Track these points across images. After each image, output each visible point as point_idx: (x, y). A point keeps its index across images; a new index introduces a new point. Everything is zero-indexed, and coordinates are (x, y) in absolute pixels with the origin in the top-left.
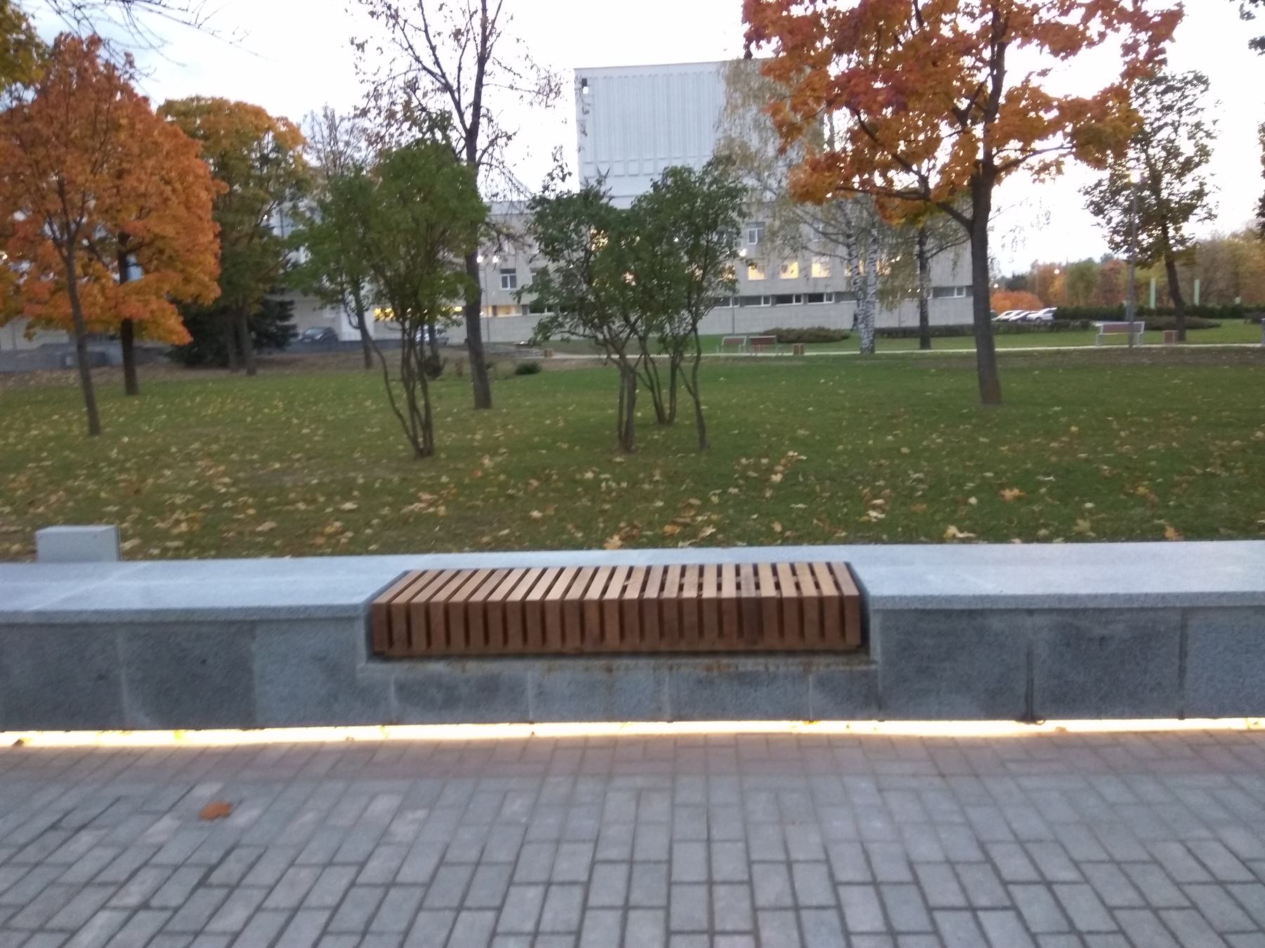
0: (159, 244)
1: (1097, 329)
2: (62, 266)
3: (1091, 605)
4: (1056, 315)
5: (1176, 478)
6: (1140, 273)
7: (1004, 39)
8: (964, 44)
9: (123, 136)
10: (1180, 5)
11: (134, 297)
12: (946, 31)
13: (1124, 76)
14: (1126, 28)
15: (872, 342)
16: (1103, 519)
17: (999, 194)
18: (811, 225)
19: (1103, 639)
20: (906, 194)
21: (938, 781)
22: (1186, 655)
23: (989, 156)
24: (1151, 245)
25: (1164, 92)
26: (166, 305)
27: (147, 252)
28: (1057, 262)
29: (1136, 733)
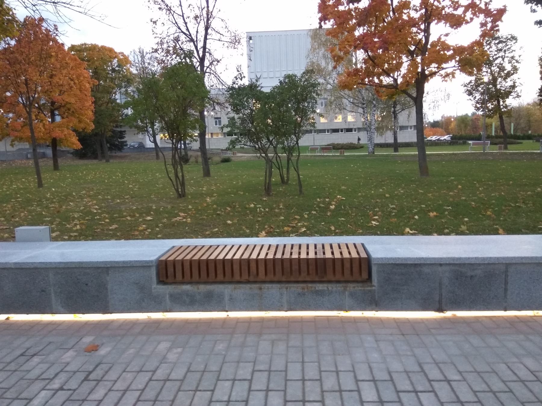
0: (68, 106)
1: (470, 144)
2: (27, 115)
3: (467, 262)
4: (452, 138)
5: (503, 208)
6: (488, 120)
7: (430, 20)
9: (53, 60)
10: (505, 6)
11: (57, 129)
12: (405, 17)
14: (482, 16)
15: (373, 149)
17: (428, 86)
19: (472, 276)
20: (388, 86)
21: (401, 337)
22: (507, 283)
24: (493, 108)
25: (498, 43)
26: (71, 132)
27: (63, 109)
28: (452, 115)
29: (486, 317)
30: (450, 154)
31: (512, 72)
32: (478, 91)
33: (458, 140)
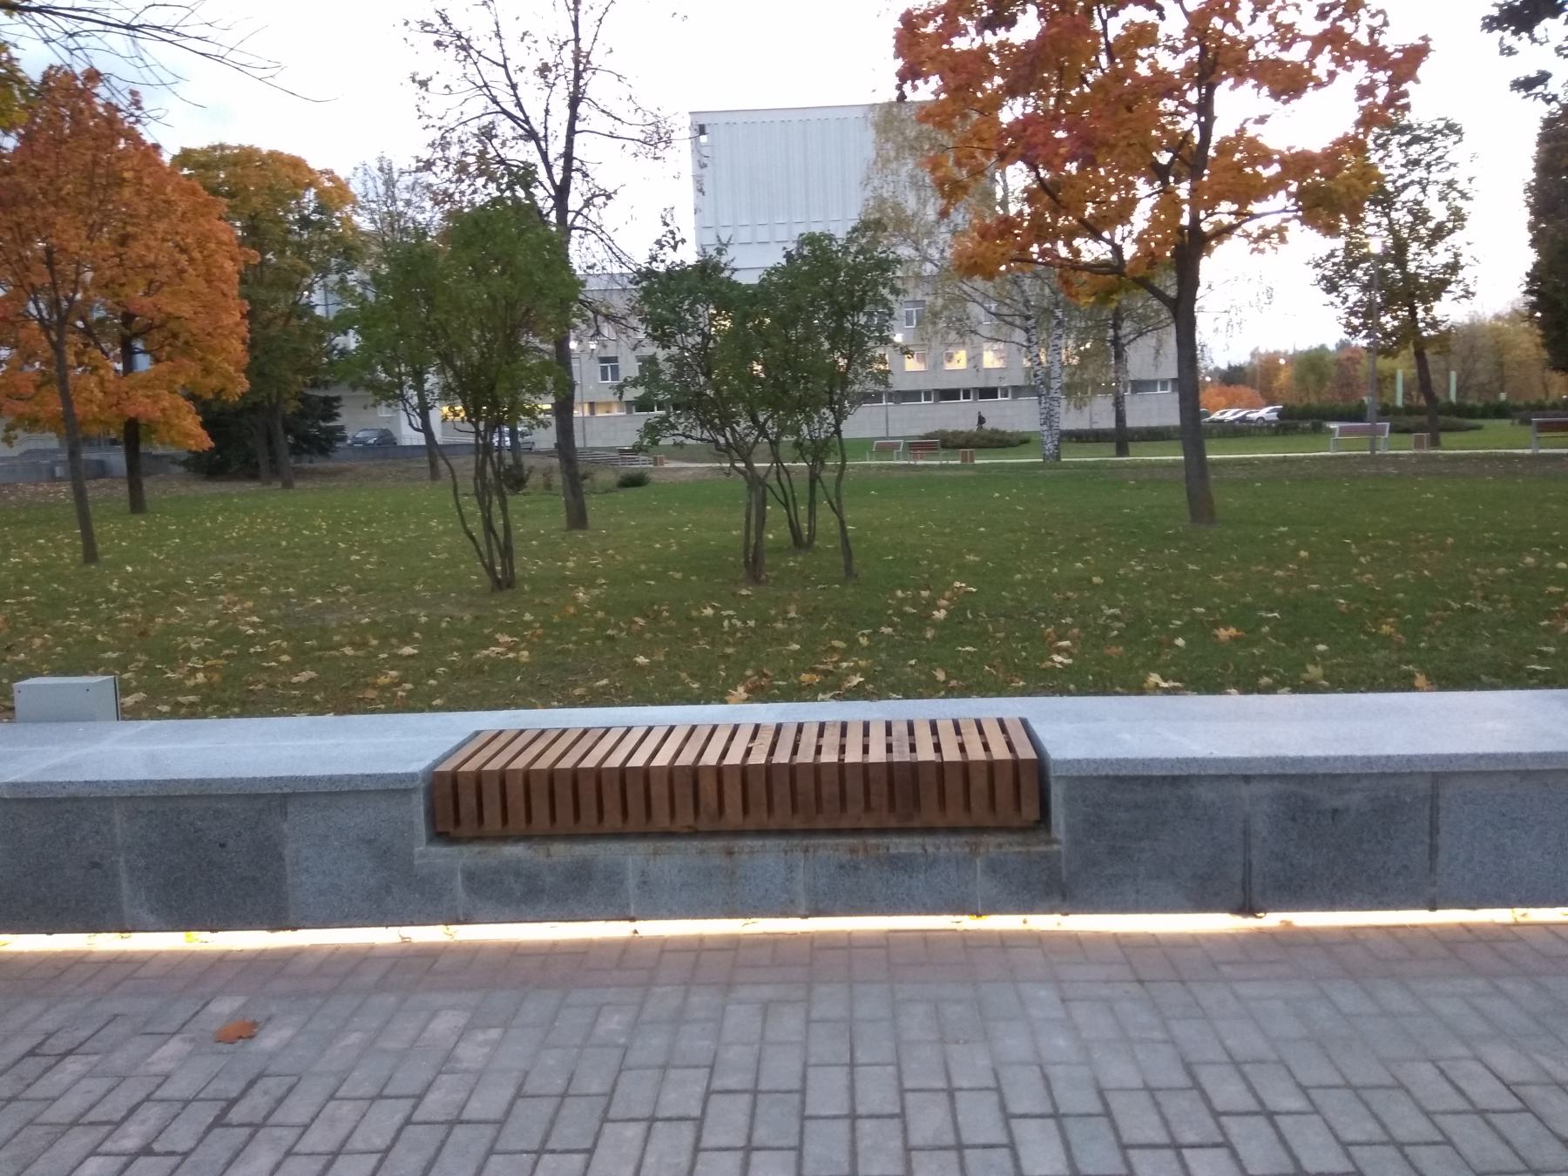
1: (1331, 431)
2: (50, 353)
3: (1321, 770)
4: (1281, 415)
5: (1428, 614)
6: (1383, 363)
8: (1164, 85)
9: (127, 193)
10: (1425, 38)
11: (140, 392)
13: (1358, 124)
14: (1361, 67)
15: (1057, 447)
16: (1339, 665)
17: (1209, 267)
18: (981, 305)
19: (1335, 811)
20: (1097, 267)
21: (1135, 988)
23: (1195, 221)
25: (1409, 144)
26: (181, 401)
27: (157, 336)
28: (1282, 349)
29: (1378, 928)
30: (1277, 461)
31: (1450, 225)
32: (1353, 278)
33: (1298, 420)
